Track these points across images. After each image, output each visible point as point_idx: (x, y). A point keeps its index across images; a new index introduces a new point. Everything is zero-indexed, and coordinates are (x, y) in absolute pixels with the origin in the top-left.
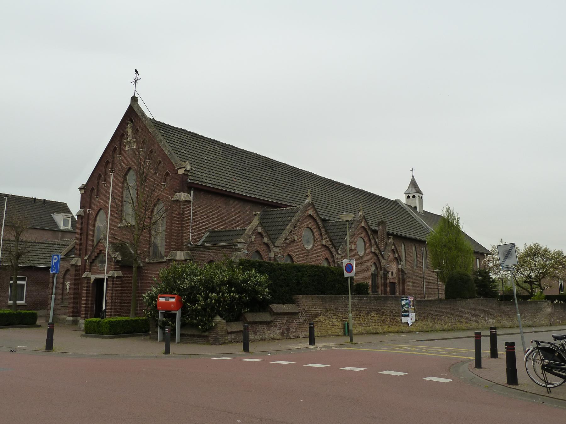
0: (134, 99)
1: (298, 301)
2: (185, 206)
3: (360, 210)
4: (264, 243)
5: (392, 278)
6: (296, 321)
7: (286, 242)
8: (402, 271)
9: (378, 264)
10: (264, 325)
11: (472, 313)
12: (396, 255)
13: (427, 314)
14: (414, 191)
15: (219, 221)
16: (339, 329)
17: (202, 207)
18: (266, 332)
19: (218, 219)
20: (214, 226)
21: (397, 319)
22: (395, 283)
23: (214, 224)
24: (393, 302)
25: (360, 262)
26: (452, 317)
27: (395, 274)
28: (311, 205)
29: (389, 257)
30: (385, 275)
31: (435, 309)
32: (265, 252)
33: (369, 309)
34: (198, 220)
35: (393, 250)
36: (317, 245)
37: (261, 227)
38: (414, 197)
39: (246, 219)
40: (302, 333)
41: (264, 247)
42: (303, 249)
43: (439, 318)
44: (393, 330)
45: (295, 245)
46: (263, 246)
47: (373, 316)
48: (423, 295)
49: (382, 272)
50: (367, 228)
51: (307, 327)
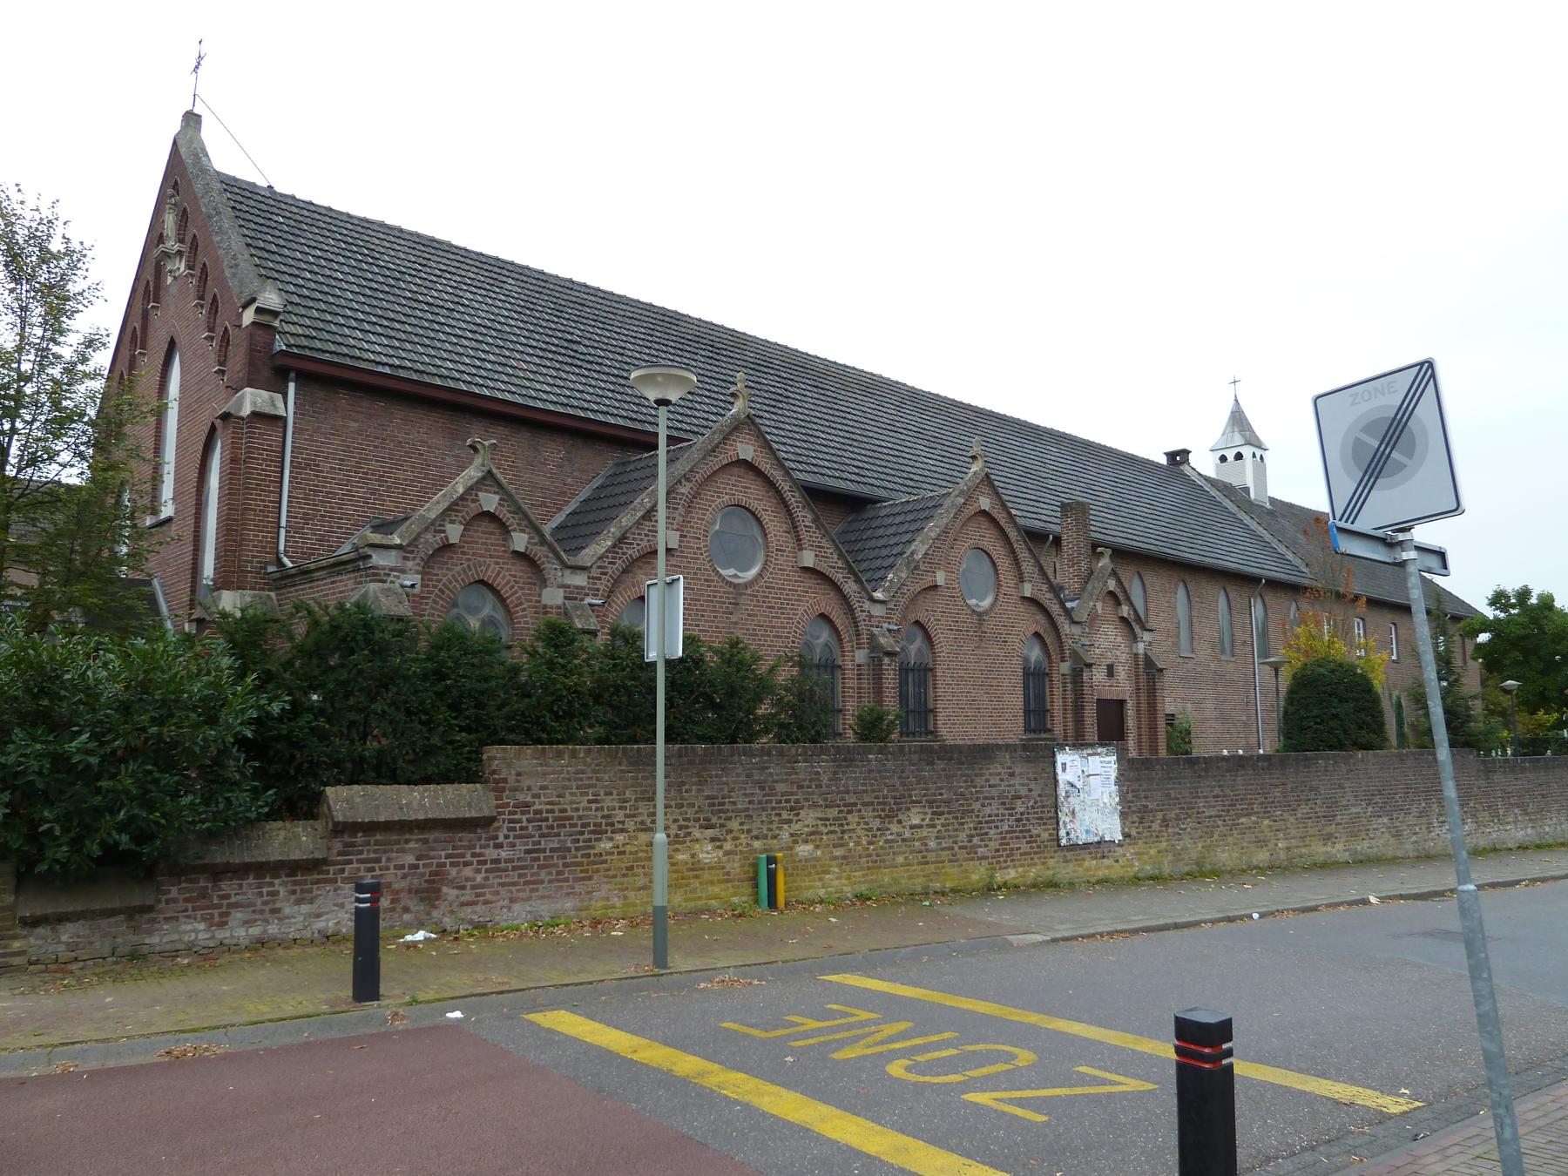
0: (192, 120)
1: (494, 772)
2: (255, 433)
3: (974, 458)
4: (517, 554)
5: (1110, 686)
6: (480, 855)
7: (624, 554)
8: (1149, 662)
9: (1049, 637)
10: (278, 877)
11: (1377, 803)
12: (1125, 610)
13: (1178, 811)
14: (1238, 439)
15: (417, 491)
16: (728, 881)
17: (343, 441)
18: (287, 911)
19: (416, 486)
20: (398, 507)
21: (1035, 832)
22: (1122, 702)
23: (397, 502)
24: (1017, 771)
25: (975, 632)
26: (1292, 819)
27: (1122, 673)
28: (749, 423)
29: (1093, 617)
30: (1077, 675)
31: (1217, 791)
32: (522, 589)
33: (895, 798)
34: (323, 487)
35: (1111, 594)
36: (780, 570)
37: (495, 493)
38: (1239, 456)
39: (542, 489)
40: (516, 907)
41: (518, 570)
42: (713, 581)
43: (1234, 825)
44: (1014, 879)
45: (675, 566)
46: (513, 564)
47: (912, 827)
48: (1253, 740)
49: (1067, 664)
50: (1002, 518)
51: (542, 882)
